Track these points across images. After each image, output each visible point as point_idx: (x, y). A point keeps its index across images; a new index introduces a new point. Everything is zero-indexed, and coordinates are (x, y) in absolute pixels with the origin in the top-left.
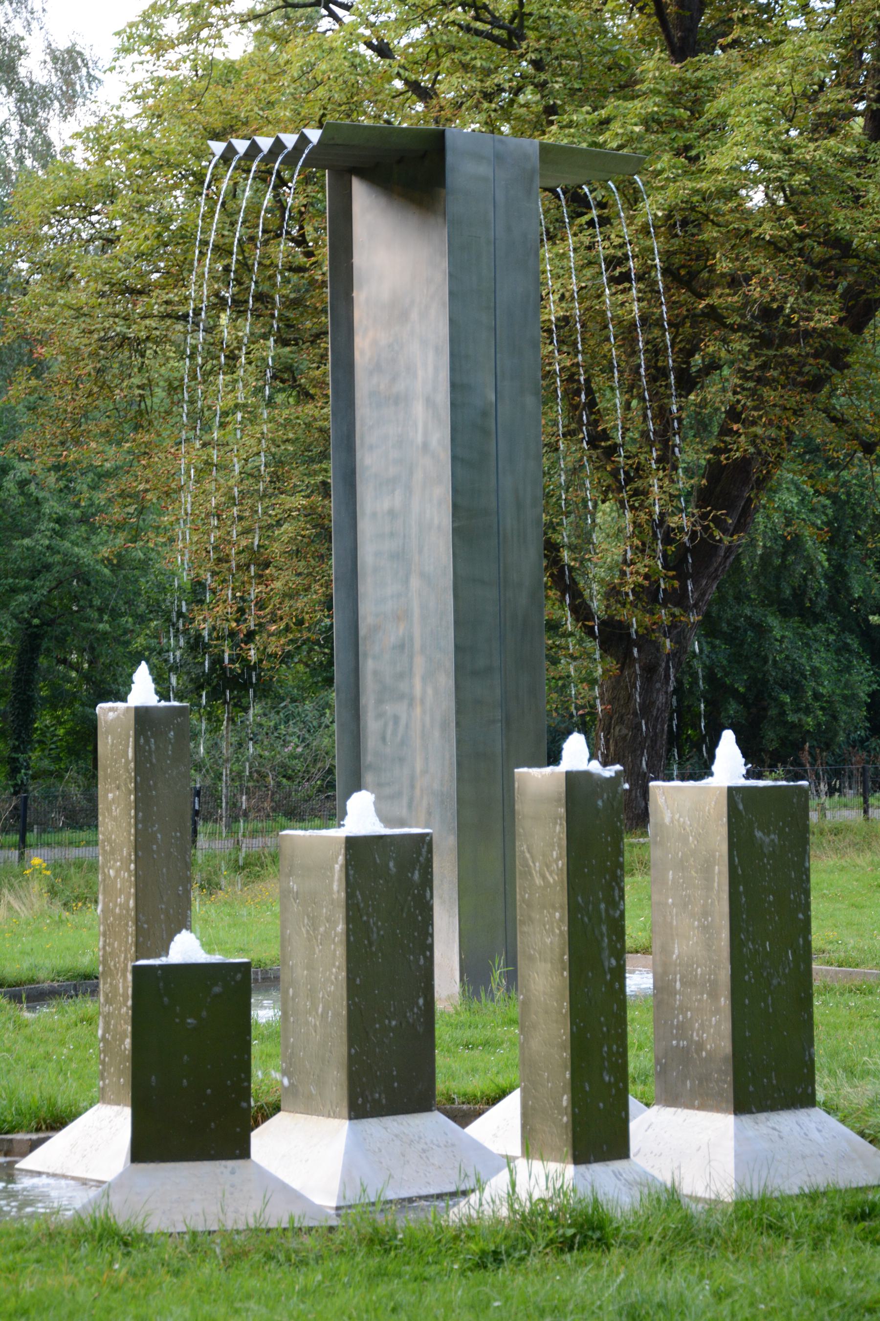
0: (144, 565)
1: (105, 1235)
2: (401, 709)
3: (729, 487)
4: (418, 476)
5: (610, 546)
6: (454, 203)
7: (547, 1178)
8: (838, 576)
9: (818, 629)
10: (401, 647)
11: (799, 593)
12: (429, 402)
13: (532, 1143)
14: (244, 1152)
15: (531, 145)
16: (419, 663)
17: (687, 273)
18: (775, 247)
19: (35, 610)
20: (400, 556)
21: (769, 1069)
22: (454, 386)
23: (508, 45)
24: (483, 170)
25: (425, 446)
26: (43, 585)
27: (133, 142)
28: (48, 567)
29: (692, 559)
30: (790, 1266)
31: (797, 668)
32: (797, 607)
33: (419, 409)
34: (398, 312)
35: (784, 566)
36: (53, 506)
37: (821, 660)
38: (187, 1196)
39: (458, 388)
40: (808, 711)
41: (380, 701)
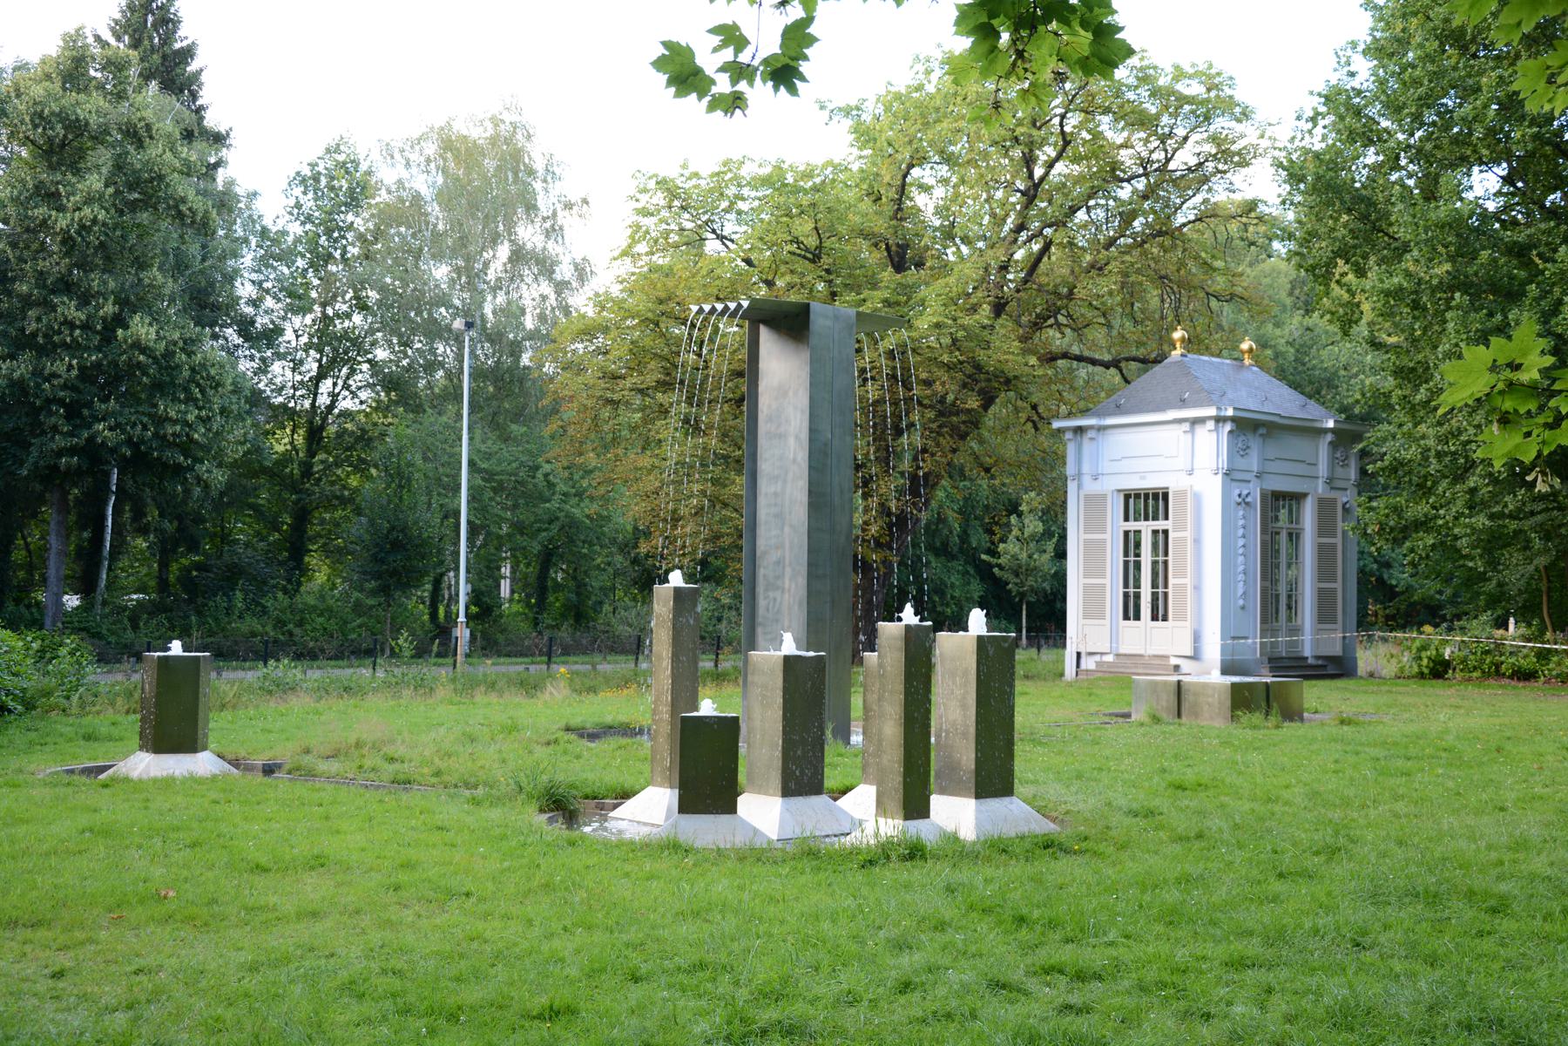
0: (608, 519)
1: (673, 847)
2: (778, 594)
3: (918, 485)
4: (790, 475)
5: (861, 514)
6: (814, 340)
7: (892, 827)
8: (964, 537)
9: (954, 563)
10: (778, 563)
11: (945, 545)
12: (797, 437)
13: (881, 808)
14: (732, 809)
15: (852, 312)
16: (788, 571)
17: (900, 379)
18: (949, 367)
19: (550, 541)
20: (779, 516)
21: (993, 779)
22: (811, 430)
23: (813, 261)
24: (829, 323)
25: (794, 460)
26: (555, 528)
27: (619, 304)
28: (557, 518)
29: (898, 523)
30: (1017, 869)
31: (943, 582)
32: (943, 551)
33: (792, 441)
34: (782, 392)
35: (937, 530)
36: (561, 487)
37: (955, 579)
38: (705, 830)
39: (813, 431)
40: (947, 605)
41: (766, 590)
